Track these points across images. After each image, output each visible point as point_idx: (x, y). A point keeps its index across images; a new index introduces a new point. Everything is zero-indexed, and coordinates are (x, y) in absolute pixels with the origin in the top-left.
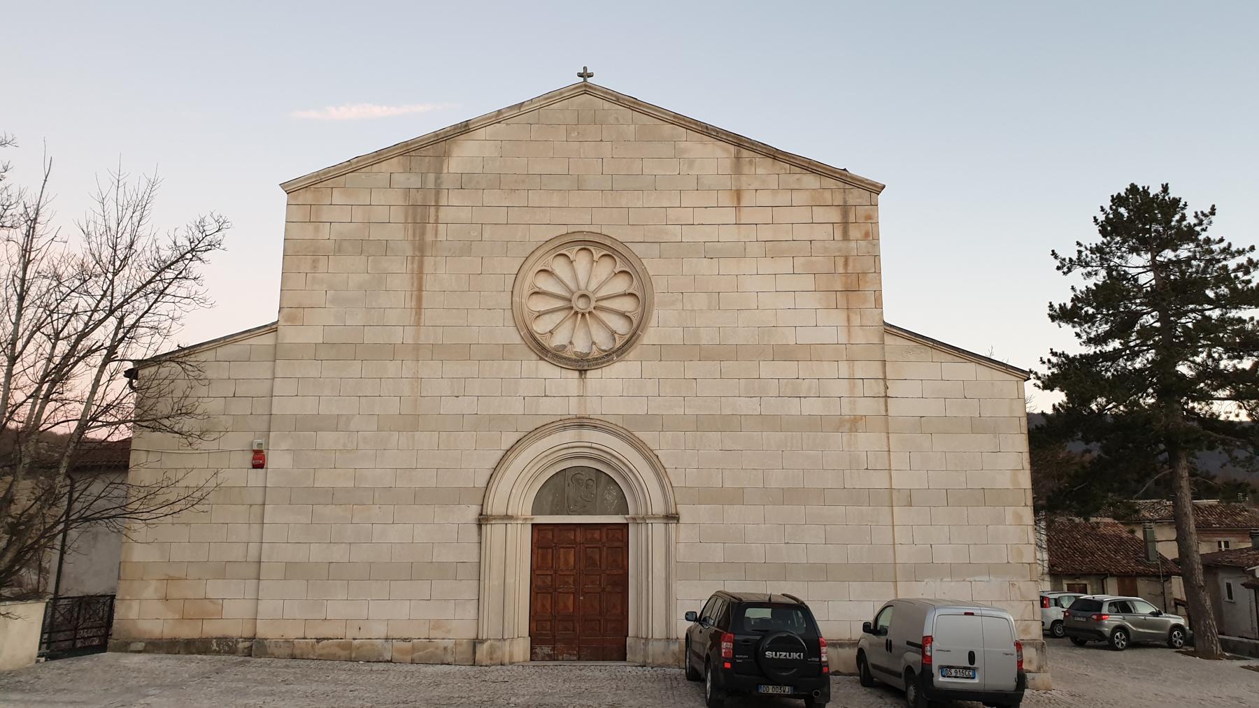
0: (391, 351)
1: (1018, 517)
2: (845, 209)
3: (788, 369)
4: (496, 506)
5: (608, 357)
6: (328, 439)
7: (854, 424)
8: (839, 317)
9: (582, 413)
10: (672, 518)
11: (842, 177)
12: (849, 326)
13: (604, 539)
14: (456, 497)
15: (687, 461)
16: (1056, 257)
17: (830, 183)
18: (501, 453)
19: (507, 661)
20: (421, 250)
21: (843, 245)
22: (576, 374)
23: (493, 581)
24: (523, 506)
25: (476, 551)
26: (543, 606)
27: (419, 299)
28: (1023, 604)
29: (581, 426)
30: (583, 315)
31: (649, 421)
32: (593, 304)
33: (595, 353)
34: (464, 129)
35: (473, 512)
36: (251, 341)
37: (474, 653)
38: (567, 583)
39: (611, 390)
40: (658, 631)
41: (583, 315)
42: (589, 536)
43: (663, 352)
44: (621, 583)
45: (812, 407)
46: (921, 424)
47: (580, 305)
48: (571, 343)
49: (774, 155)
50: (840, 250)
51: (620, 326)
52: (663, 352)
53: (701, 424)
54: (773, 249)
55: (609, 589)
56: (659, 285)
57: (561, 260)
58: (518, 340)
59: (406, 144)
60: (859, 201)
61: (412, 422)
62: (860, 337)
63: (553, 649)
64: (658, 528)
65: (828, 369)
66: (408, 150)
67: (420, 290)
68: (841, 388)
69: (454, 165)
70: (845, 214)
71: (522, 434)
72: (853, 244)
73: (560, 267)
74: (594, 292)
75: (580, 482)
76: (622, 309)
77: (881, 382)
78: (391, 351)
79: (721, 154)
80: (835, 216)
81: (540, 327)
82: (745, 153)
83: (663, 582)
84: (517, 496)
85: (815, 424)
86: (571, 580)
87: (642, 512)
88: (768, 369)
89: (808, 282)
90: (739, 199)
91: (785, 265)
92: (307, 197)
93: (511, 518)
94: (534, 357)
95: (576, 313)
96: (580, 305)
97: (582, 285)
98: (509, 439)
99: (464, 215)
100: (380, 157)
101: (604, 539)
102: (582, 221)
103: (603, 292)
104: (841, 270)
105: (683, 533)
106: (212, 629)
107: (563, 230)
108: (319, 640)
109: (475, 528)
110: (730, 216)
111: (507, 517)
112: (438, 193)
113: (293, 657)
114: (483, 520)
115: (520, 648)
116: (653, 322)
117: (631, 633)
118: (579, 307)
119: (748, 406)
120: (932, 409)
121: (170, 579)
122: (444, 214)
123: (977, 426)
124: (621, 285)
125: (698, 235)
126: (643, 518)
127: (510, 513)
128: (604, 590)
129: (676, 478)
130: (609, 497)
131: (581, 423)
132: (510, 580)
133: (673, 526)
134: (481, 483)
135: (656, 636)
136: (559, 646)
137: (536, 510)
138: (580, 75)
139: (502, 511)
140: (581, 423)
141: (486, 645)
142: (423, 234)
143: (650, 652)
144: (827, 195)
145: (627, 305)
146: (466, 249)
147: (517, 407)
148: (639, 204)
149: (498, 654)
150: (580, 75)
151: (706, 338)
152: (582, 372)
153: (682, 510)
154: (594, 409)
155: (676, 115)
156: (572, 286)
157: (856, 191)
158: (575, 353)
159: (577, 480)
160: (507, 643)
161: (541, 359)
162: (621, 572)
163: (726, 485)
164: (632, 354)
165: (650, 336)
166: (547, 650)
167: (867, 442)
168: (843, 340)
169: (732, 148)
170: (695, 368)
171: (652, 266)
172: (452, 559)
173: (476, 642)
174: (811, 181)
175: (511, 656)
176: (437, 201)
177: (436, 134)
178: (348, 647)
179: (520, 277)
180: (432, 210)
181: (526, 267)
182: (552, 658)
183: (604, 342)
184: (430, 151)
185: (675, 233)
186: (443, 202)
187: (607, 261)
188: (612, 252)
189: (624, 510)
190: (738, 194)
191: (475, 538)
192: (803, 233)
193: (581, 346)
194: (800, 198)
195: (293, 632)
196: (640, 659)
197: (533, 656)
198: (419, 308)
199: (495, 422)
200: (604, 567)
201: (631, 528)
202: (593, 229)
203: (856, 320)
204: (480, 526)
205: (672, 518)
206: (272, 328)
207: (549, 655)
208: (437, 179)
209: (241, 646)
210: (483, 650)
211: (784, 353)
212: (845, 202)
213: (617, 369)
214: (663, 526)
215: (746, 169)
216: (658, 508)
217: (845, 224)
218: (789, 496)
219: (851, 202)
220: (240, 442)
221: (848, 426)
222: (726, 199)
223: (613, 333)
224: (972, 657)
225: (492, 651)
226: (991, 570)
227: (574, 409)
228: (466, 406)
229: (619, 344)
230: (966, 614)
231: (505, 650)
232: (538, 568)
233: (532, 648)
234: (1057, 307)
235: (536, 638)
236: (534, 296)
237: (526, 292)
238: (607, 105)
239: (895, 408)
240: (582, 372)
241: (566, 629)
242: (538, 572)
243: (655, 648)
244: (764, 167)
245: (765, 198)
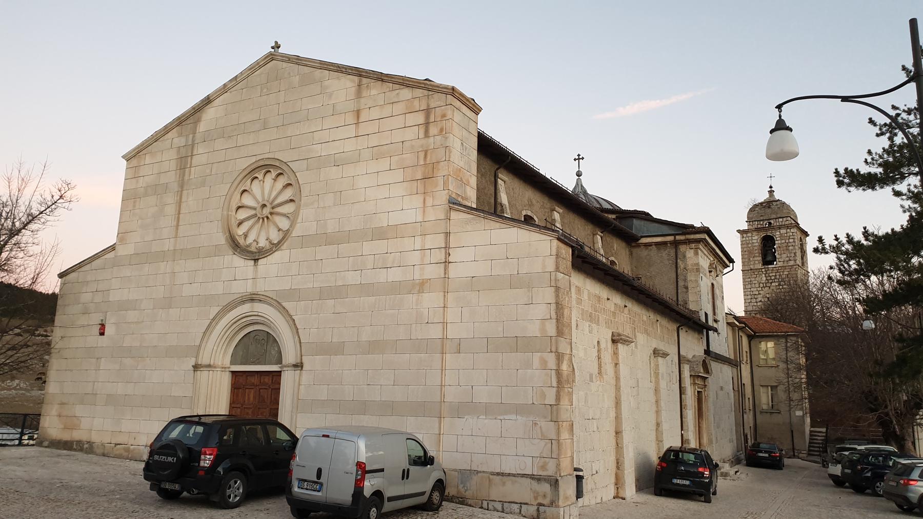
0: (162, 256)
1: (544, 362)
2: (428, 111)
3: (381, 246)
6: (132, 315)
7: (421, 286)
8: (417, 201)
9: (254, 291)
10: (299, 366)
11: (427, 86)
12: (424, 207)
15: (315, 322)
16: (875, 125)
17: (419, 92)
20: (182, 185)
21: (424, 141)
27: (178, 218)
28: (543, 443)
29: (252, 300)
30: (268, 218)
31: (294, 294)
34: (207, 101)
36: (106, 256)
38: (247, 414)
39: (272, 274)
41: (268, 218)
45: (395, 275)
46: (473, 284)
47: (266, 211)
49: (381, 78)
50: (422, 146)
53: (325, 293)
54: (378, 153)
56: (305, 190)
59: (179, 118)
60: (438, 103)
61: (168, 303)
62: (432, 215)
65: (407, 243)
66: (180, 121)
67: (179, 213)
68: (415, 258)
69: (202, 127)
70: (427, 117)
72: (431, 139)
77: (443, 250)
78: (162, 256)
79: (349, 83)
80: (420, 118)
82: (365, 80)
85: (396, 288)
86: (250, 412)
88: (368, 247)
89: (399, 175)
90: (358, 117)
91: (384, 164)
92: (134, 162)
96: (266, 211)
97: (260, 200)
98: (214, 311)
100: (167, 130)
102: (263, 152)
104: (422, 162)
105: (306, 377)
106: (77, 435)
107: (254, 159)
108: (116, 444)
110: (351, 131)
112: (193, 146)
113: (104, 455)
114: (196, 367)
119: (352, 278)
120: (481, 270)
121: (63, 404)
123: (516, 282)
125: (332, 149)
131: (252, 298)
137: (232, 363)
138: (273, 48)
139: (208, 363)
142: (184, 175)
144: (416, 103)
150: (273, 48)
151: (331, 227)
152: (256, 260)
154: (262, 287)
155: (321, 62)
157: (436, 96)
163: (334, 340)
167: (431, 300)
168: (420, 219)
169: (356, 79)
174: (406, 93)
177: (193, 108)
178: (127, 450)
183: (275, 237)
184: (191, 120)
189: (279, 361)
190: (358, 113)
192: (398, 137)
194: (399, 108)
195: (106, 440)
198: (178, 225)
203: (429, 201)
206: (113, 248)
208: (193, 137)
209: (86, 446)
211: (380, 234)
212: (428, 106)
215: (364, 94)
217: (427, 124)
218: (374, 347)
219: (432, 105)
220: (96, 319)
221: (418, 288)
222: (351, 119)
224: (319, 472)
226: (519, 409)
227: (249, 288)
230: (324, 436)
234: (842, 172)
238: (285, 65)
239: (453, 271)
240: (256, 260)
244: (375, 90)
245: (375, 114)
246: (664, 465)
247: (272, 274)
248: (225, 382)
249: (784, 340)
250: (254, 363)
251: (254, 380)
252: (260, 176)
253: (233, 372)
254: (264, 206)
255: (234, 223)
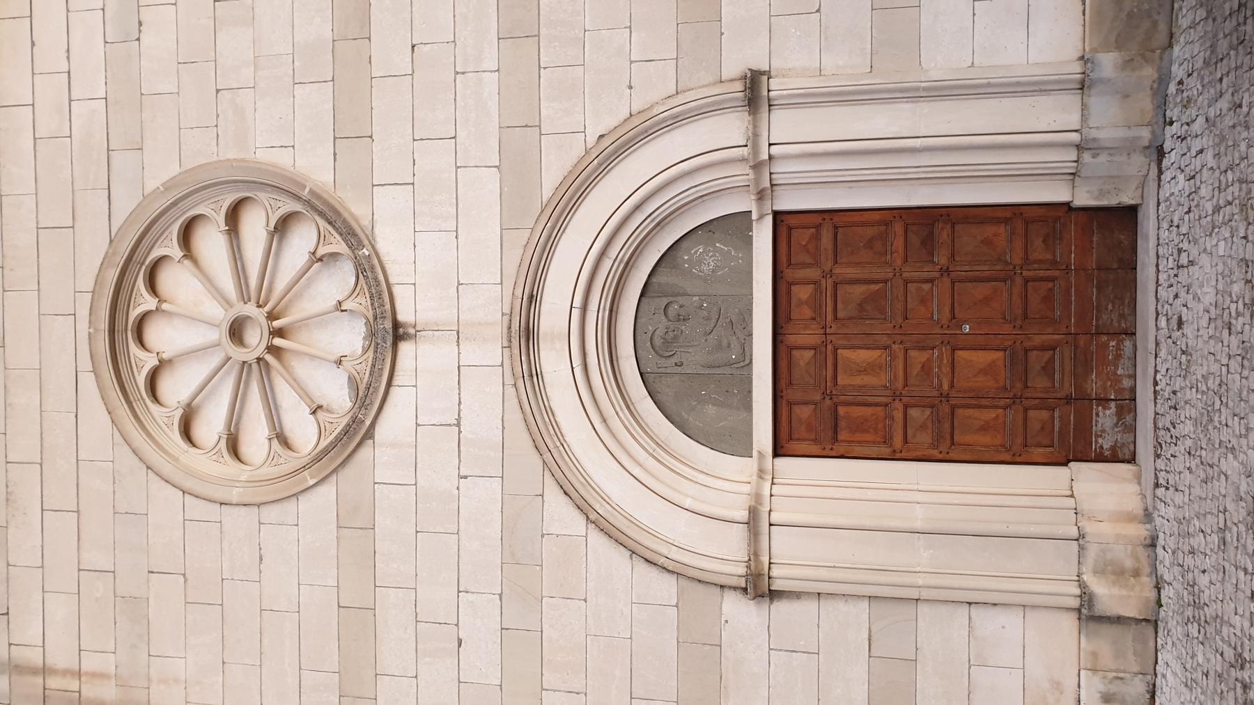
4: (725, 552)
5: (372, 277)
10: (754, 91)
13: (813, 273)
14: (702, 651)
15: (611, 67)
18: (596, 538)
19: (1140, 531)
22: (405, 348)
23: (921, 563)
24: (727, 479)
25: (842, 606)
26: (984, 428)
30: (280, 333)
31: (514, 166)
32: (250, 310)
33: (361, 303)
35: (737, 609)
37: (1119, 620)
38: (926, 368)
39: (447, 262)
40: (1059, 114)
41: (280, 333)
42: (808, 312)
43: (350, 134)
44: (926, 223)
47: (256, 338)
48: (339, 362)
51: (302, 241)
52: (350, 134)
55: (941, 258)
56: (203, 151)
57: (166, 386)
58: (327, 492)
63: (1104, 401)
64: (784, 126)
71: (549, 480)
73: (176, 389)
74: (227, 303)
75: (668, 337)
76: (262, 236)
81: (306, 434)
83: (925, 108)
84: (698, 493)
86: (918, 357)
87: (743, 174)
93: (753, 512)
94: (365, 453)
95: (271, 349)
96: (256, 338)
98: (561, 516)
99: (61, 609)
101: (813, 273)
103: (228, 284)
105: (794, 62)
107: (88, 381)
109: (781, 608)
111: (753, 522)
114: (759, 587)
115: (1102, 490)
116: (282, 159)
117: (1056, 193)
118: (262, 341)
122: (61, 657)
124: (212, 242)
126: (757, 167)
127: (743, 515)
128: (946, 271)
129: (655, 88)
130: (709, 264)
131: (525, 334)
132: (918, 518)
133: (777, 87)
134: (666, 587)
135: (1074, 120)
136: (1094, 385)
137: (738, 444)
140: (525, 334)
141: (1100, 588)
143: (1121, 133)
145: (255, 226)
146: (133, 608)
147: (483, 497)
148: (30, 202)
149: (1123, 555)
152: (399, 333)
153: (735, 64)
154: (489, 304)
156: (215, 360)
158: (365, 351)
159: (667, 343)
160: (1090, 528)
161: (369, 434)
162: (898, 228)
164: (356, 208)
165: (315, 167)
166: (1105, 418)
170: (388, 49)
171: (160, 169)
172: (859, 670)
173: (1088, 613)
175: (1130, 518)
176: (34, 671)
179: (188, 484)
180: (53, 683)
181: (167, 469)
182: (1127, 405)
183: (337, 283)
185: (89, 115)
186: (33, 657)
187: (169, 279)
188: (134, 276)
191: (807, 608)
193: (350, 337)
196: (1138, 164)
197: (1122, 455)
199: (519, 552)
200: (886, 273)
201: (787, 203)
202: (83, 312)
204: (774, 595)
205: (754, 91)
207: (1120, 414)
210: (1108, 596)
213: (391, 245)
214: (777, 115)
216: (729, 130)
223: (316, 258)
225: (1117, 573)
227: (489, 352)
228: (481, 621)
229: (337, 245)
231: (1114, 533)
232: (887, 440)
233: (1100, 458)
235: (1072, 447)
236: (243, 458)
237: (229, 467)
240: (399, 333)
241: (1048, 369)
242: (898, 441)
243: (1109, 119)
246: (1110, 317)
247: (447, 262)
248: (816, 483)
249: (795, 352)
250: (746, 362)
251: (804, 336)
252: (149, 303)
253: (777, 453)
254: (236, 331)
255: (289, 462)
